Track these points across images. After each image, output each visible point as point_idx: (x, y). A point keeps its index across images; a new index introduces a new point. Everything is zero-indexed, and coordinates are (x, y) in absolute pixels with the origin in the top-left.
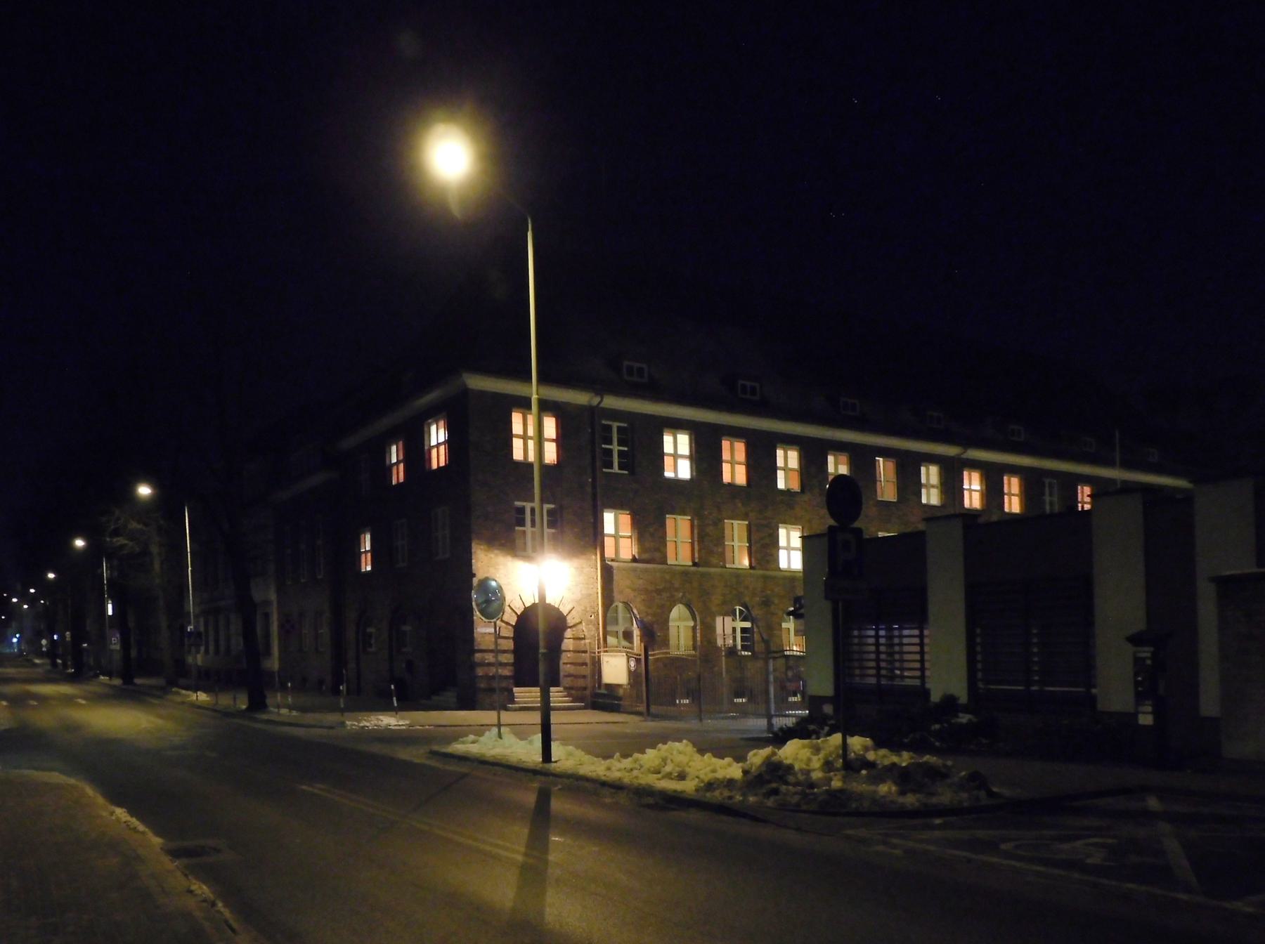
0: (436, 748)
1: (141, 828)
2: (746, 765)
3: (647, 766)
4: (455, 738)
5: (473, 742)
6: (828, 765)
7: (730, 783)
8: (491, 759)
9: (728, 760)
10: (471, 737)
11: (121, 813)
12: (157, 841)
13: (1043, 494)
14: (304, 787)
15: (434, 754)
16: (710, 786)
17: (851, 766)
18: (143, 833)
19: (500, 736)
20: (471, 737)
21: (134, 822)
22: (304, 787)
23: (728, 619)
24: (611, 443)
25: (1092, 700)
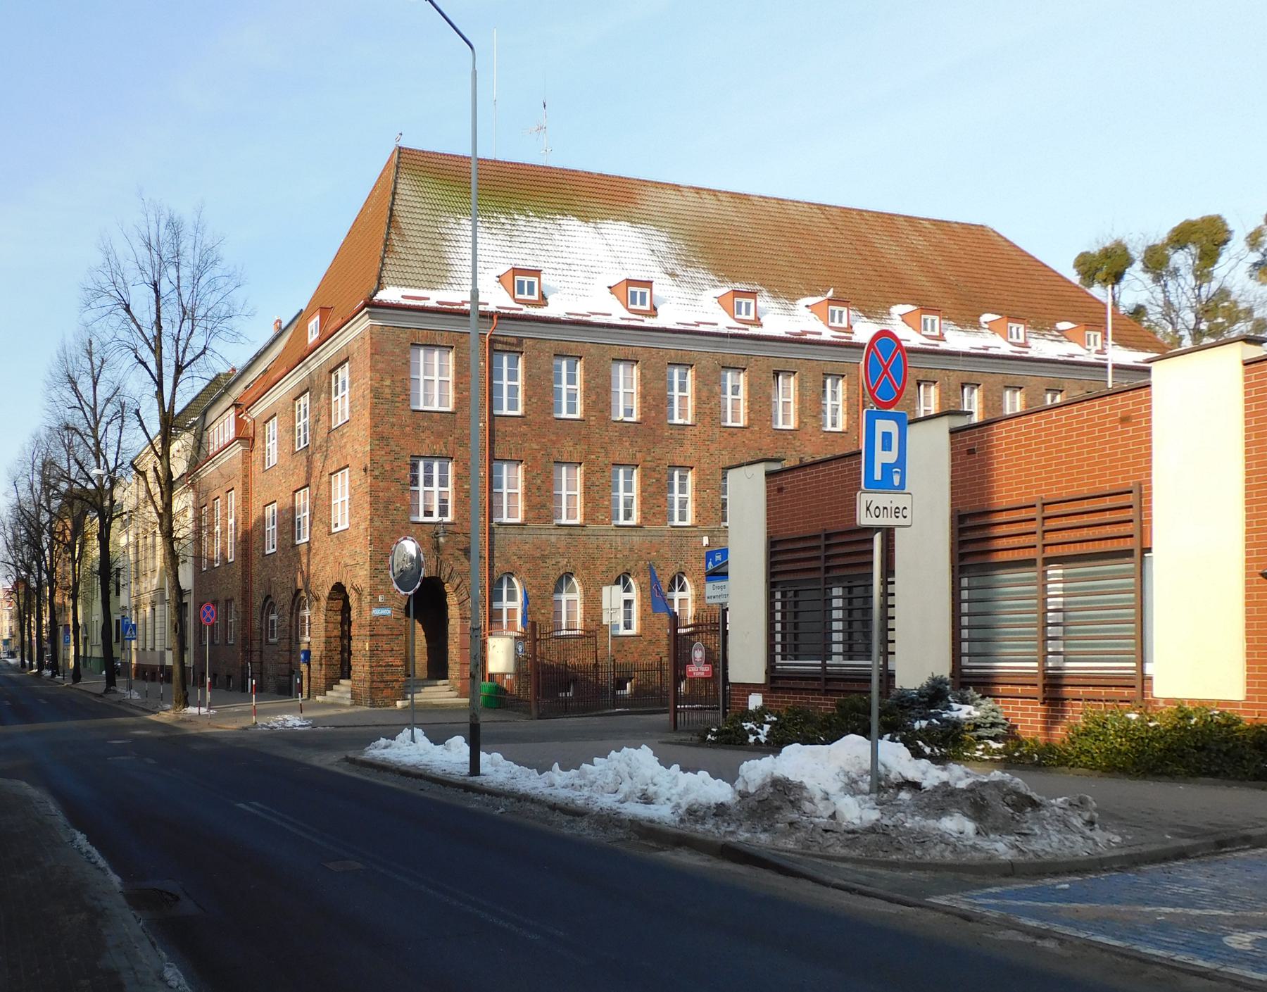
0: (351, 754)
1: (102, 863)
2: (740, 785)
3: (844, 827)
4: (370, 739)
5: (386, 747)
6: (851, 787)
7: (720, 810)
8: (413, 770)
9: (703, 774)
10: (383, 741)
11: (81, 838)
12: (116, 879)
13: (670, 488)
14: (241, 805)
15: (352, 761)
16: (693, 813)
17: (882, 786)
18: (102, 870)
19: (413, 740)
20: (383, 741)
21: (94, 852)
22: (241, 805)
23: (618, 589)
24: (509, 386)
25: (1145, 680)
